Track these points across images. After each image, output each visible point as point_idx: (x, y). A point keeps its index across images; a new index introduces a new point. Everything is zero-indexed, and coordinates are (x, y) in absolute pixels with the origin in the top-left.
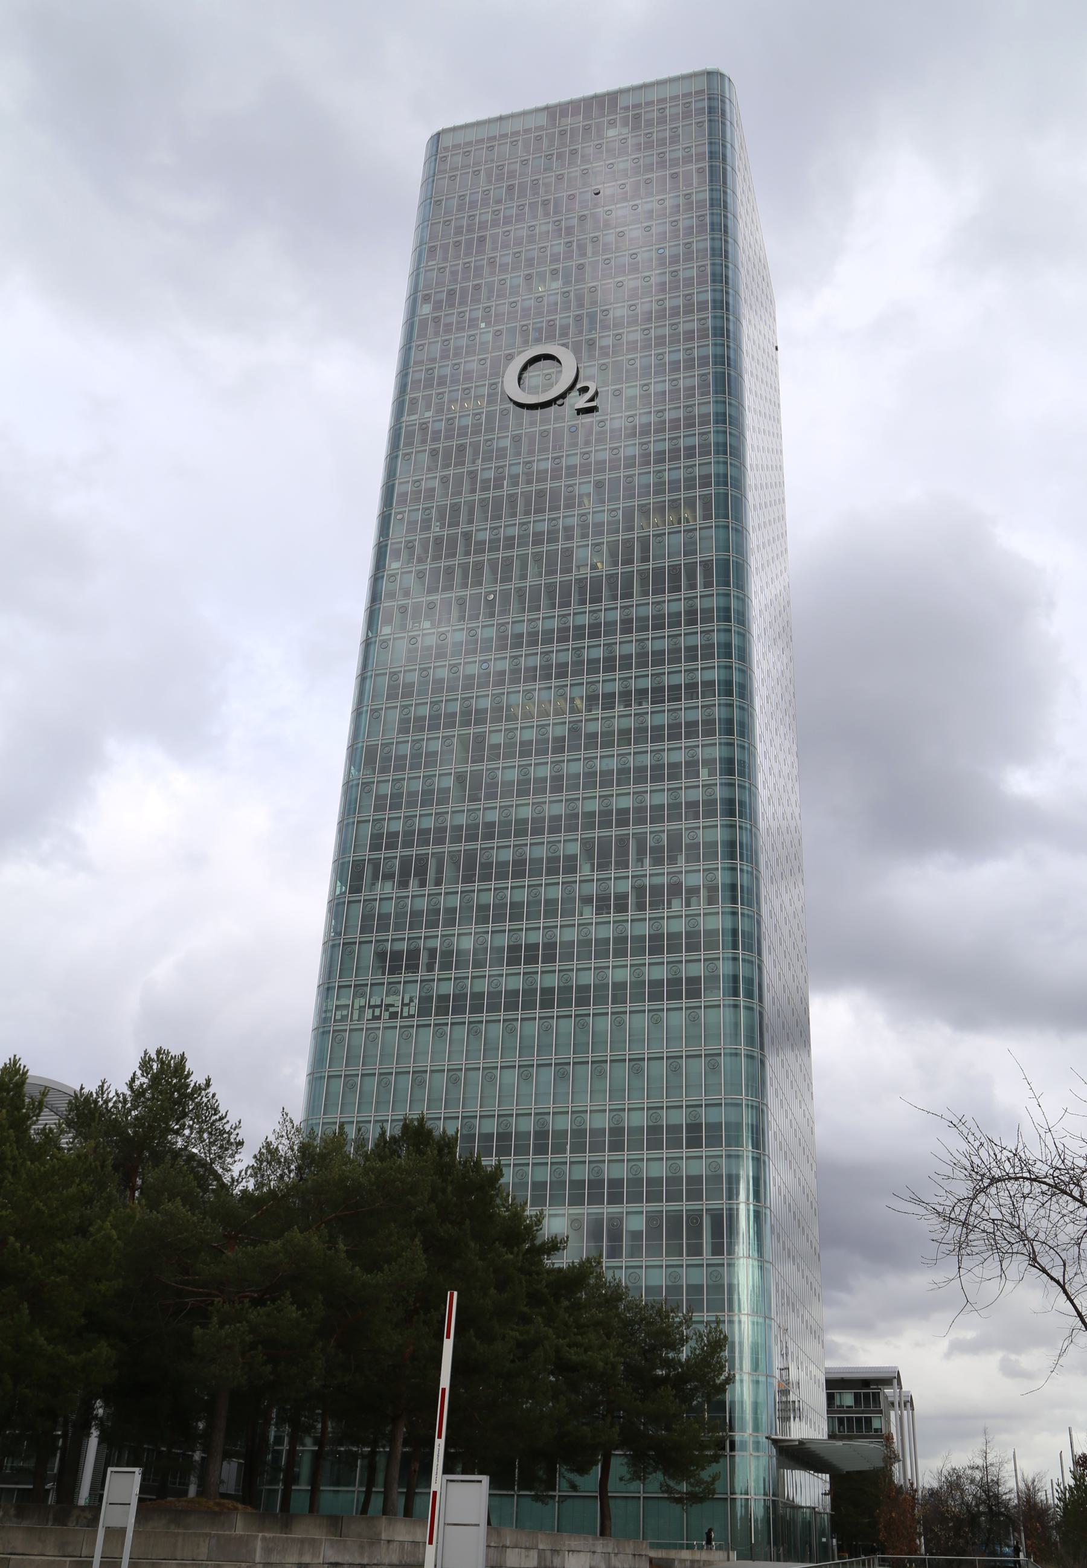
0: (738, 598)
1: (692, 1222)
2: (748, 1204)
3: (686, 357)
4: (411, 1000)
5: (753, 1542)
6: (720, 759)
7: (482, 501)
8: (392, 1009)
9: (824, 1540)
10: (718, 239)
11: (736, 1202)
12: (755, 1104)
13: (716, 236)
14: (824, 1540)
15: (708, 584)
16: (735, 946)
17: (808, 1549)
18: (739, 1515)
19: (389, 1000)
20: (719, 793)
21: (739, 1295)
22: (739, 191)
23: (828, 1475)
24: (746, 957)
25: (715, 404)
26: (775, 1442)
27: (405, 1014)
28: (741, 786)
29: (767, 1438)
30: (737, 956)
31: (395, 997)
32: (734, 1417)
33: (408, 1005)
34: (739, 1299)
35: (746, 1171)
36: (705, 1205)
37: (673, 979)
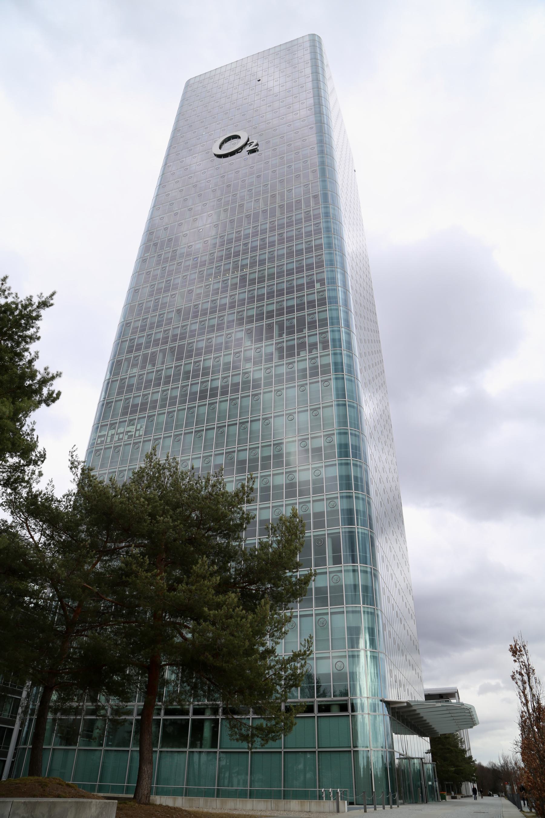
0: (365, 572)
1: (318, 544)
2: (366, 651)
3: (311, 365)
4: (141, 427)
5: (374, 790)
6: (342, 510)
7: (171, 348)
8: (129, 434)
9: (430, 783)
10: (334, 309)
11: (356, 649)
12: (369, 610)
13: (333, 307)
14: (430, 783)
15: (337, 560)
16: (354, 561)
17: (420, 791)
18: (362, 767)
19: (128, 429)
20: (340, 505)
21: (359, 682)
22: (342, 208)
23: (428, 738)
24: (353, 432)
25: (331, 333)
26: (388, 704)
27: (137, 435)
28: (355, 465)
29: (381, 701)
30: (356, 568)
31: (132, 427)
32: (356, 704)
33: (139, 430)
34: (360, 684)
35: (364, 622)
36: (326, 531)
37: (304, 515)
